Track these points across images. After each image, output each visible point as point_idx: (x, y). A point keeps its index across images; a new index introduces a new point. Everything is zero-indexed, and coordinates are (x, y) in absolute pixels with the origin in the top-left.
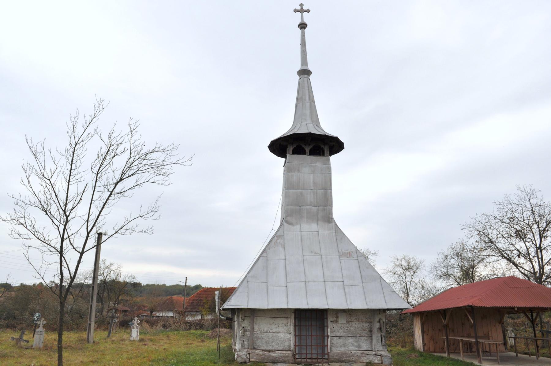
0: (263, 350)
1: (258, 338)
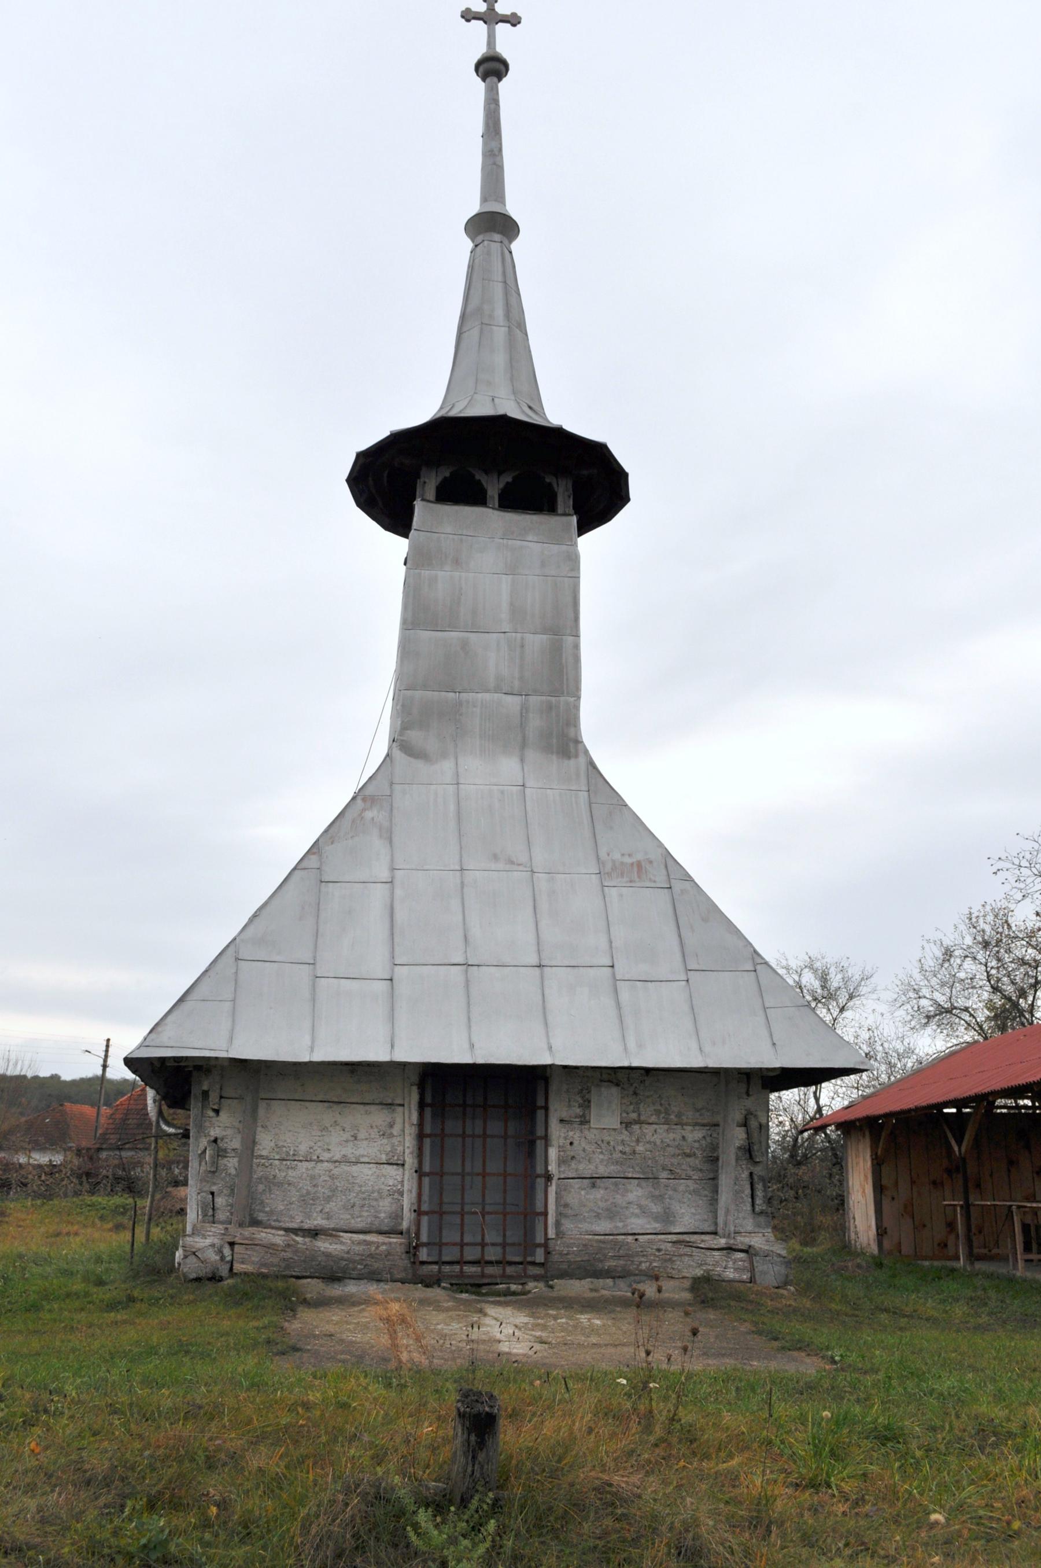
0: (287, 1230)
1: (272, 1183)
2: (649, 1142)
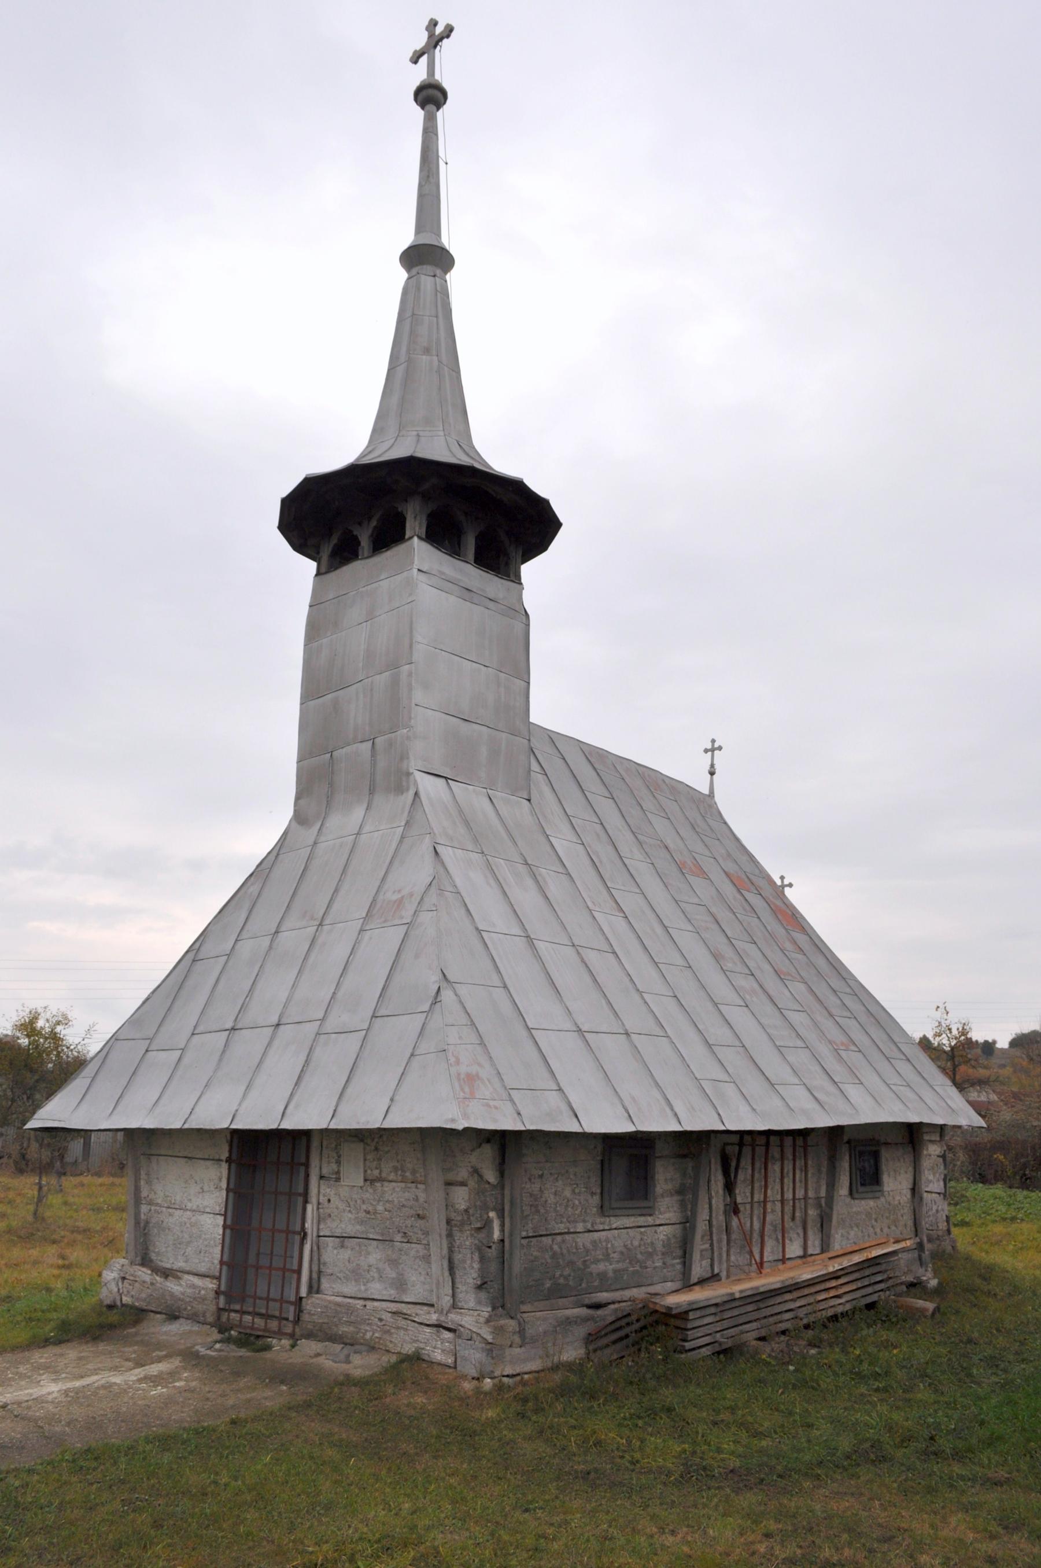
2: (388, 1201)
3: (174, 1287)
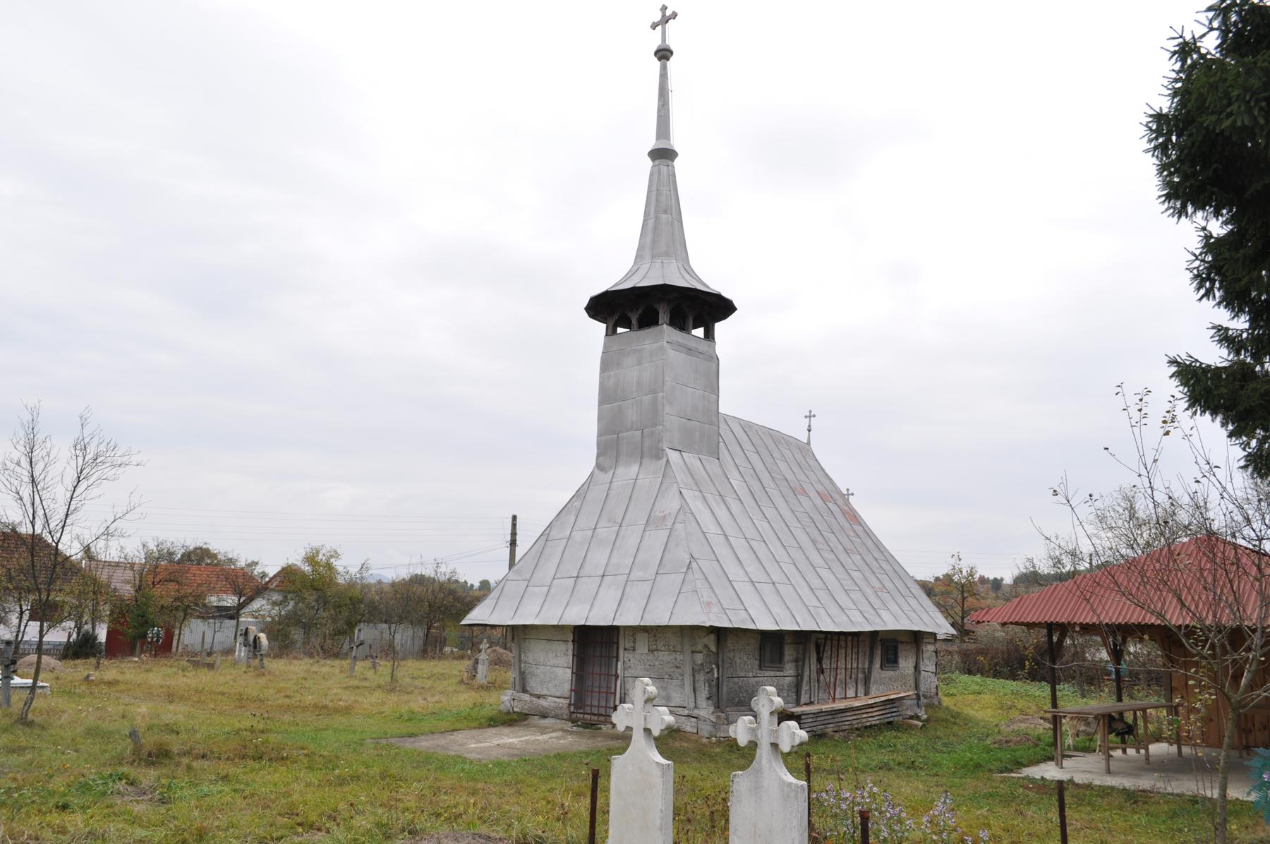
3: (542, 702)
